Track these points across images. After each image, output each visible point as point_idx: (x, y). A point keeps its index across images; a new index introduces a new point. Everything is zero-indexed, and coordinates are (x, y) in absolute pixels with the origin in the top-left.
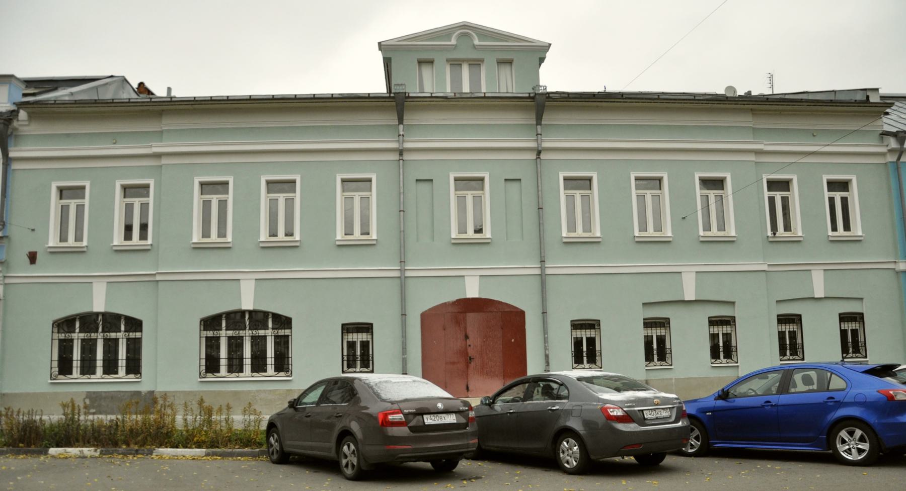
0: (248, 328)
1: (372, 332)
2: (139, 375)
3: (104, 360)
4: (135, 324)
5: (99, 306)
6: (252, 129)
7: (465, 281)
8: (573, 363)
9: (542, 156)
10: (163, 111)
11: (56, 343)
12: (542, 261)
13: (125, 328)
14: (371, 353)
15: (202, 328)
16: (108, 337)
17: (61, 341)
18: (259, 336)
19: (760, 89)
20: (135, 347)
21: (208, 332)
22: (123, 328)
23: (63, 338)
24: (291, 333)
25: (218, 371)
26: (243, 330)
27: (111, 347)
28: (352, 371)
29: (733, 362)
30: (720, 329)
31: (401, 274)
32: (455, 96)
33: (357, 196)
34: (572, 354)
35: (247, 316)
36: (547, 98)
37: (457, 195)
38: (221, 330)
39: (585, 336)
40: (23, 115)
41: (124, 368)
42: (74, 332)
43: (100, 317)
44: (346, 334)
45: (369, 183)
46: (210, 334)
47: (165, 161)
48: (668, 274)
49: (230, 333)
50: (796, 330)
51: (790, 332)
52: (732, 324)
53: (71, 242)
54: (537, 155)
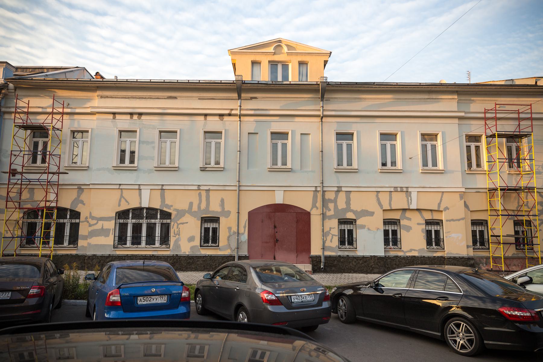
1: (219, 223)
14: (218, 235)
15: (117, 218)
16: (59, 222)
19: (463, 80)
22: (68, 217)
26: (142, 219)
27: (151, 228)
29: (354, 248)
32: (272, 83)
33: (280, 143)
34: (338, 240)
36: (327, 85)
37: (282, 143)
38: (129, 219)
39: (434, 229)
42: (129, 219)
45: (176, 133)
46: (122, 221)
49: (134, 221)
50: (484, 229)
51: (479, 231)
52: (440, 224)
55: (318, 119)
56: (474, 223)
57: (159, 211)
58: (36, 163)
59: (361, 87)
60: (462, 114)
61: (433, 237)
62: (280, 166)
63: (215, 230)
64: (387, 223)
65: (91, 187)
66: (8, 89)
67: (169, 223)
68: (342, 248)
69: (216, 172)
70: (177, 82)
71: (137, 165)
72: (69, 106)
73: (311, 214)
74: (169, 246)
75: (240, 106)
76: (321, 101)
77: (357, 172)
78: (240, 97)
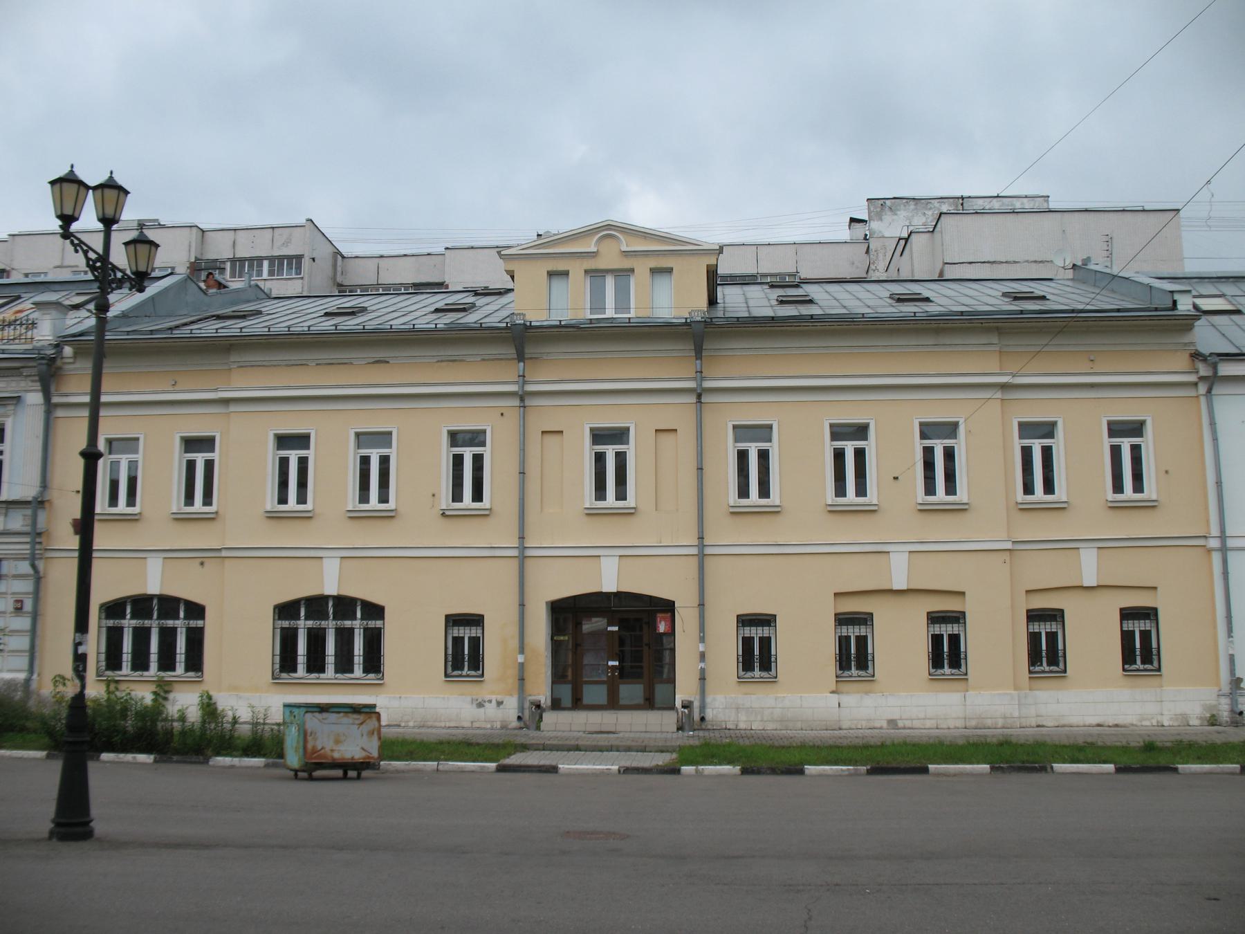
0: (331, 618)
2: (200, 673)
3: (336, 655)
4: (196, 610)
5: (153, 587)
6: (1240, 359)
8: (931, 667)
9: (528, 403)
10: (231, 345)
11: (104, 631)
12: (522, 538)
13: (361, 616)
14: (481, 653)
15: (277, 617)
17: (110, 629)
18: (344, 628)
20: (196, 640)
21: (283, 622)
23: (112, 625)
24: (384, 624)
25: (295, 670)
28: (457, 674)
30: (467, 631)
31: (519, 553)
34: (929, 656)
35: (330, 604)
40: (68, 351)
41: (183, 665)
42: (299, 619)
43: (155, 602)
44: (742, 628)
46: (286, 624)
47: (233, 408)
49: (310, 623)
50: (1148, 629)
54: (697, 398)
56: (1034, 616)
57: (359, 603)
58: (462, 501)
61: (757, 652)
62: (611, 502)
63: (476, 643)
65: (224, 554)
67: (380, 628)
68: (745, 676)
70: (560, 326)
74: (381, 675)
76: (697, 359)
77: (966, 510)
78: (521, 357)
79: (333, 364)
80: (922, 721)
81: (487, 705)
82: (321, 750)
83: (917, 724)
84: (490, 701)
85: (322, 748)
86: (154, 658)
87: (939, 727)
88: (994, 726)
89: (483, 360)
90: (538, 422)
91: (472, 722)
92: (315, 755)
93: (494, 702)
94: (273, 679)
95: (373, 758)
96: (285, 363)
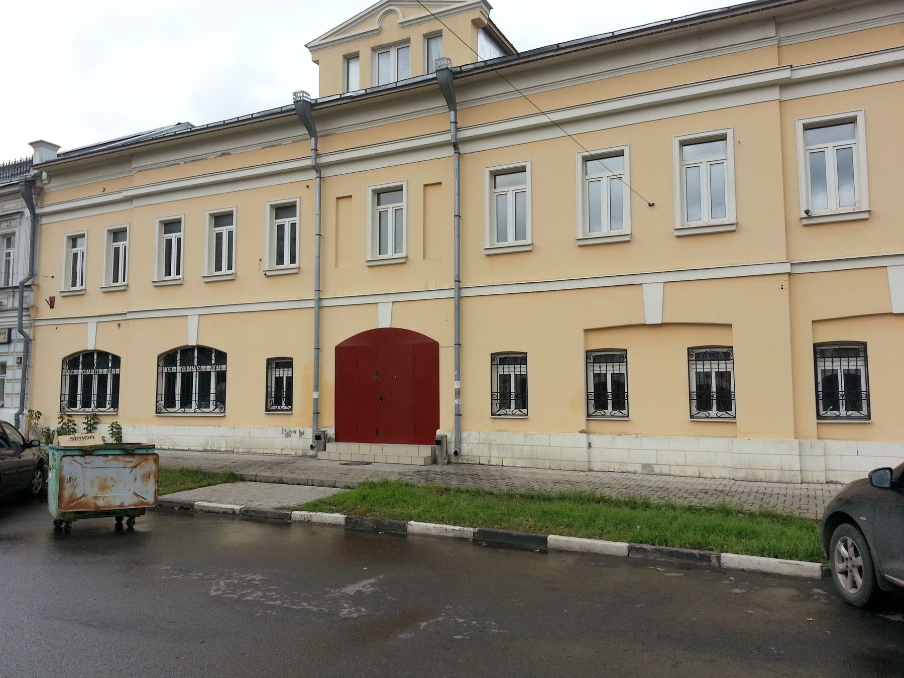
7: (378, 309)
14: (863, 388)
29: (622, 415)
34: (734, 396)
35: (214, 354)
47: (136, 203)
48: (711, 281)
53: (390, 253)
55: (450, 151)
59: (528, 62)
60: (785, 74)
64: (828, 354)
66: (42, 181)
69: (609, 247)
71: (629, 228)
72: (106, 192)
73: (440, 346)
75: (316, 150)
76: (450, 110)
79: (195, 161)
80: (681, 467)
81: (292, 434)
82: (81, 498)
83: (675, 471)
84: (295, 432)
85: (84, 495)
86: (178, 398)
87: (701, 476)
88: (768, 480)
89: (294, 142)
90: (334, 189)
91: (282, 450)
92: (72, 504)
93: (298, 433)
94: (156, 413)
95: (148, 503)
96: (165, 164)
